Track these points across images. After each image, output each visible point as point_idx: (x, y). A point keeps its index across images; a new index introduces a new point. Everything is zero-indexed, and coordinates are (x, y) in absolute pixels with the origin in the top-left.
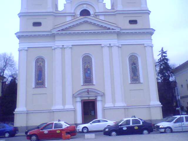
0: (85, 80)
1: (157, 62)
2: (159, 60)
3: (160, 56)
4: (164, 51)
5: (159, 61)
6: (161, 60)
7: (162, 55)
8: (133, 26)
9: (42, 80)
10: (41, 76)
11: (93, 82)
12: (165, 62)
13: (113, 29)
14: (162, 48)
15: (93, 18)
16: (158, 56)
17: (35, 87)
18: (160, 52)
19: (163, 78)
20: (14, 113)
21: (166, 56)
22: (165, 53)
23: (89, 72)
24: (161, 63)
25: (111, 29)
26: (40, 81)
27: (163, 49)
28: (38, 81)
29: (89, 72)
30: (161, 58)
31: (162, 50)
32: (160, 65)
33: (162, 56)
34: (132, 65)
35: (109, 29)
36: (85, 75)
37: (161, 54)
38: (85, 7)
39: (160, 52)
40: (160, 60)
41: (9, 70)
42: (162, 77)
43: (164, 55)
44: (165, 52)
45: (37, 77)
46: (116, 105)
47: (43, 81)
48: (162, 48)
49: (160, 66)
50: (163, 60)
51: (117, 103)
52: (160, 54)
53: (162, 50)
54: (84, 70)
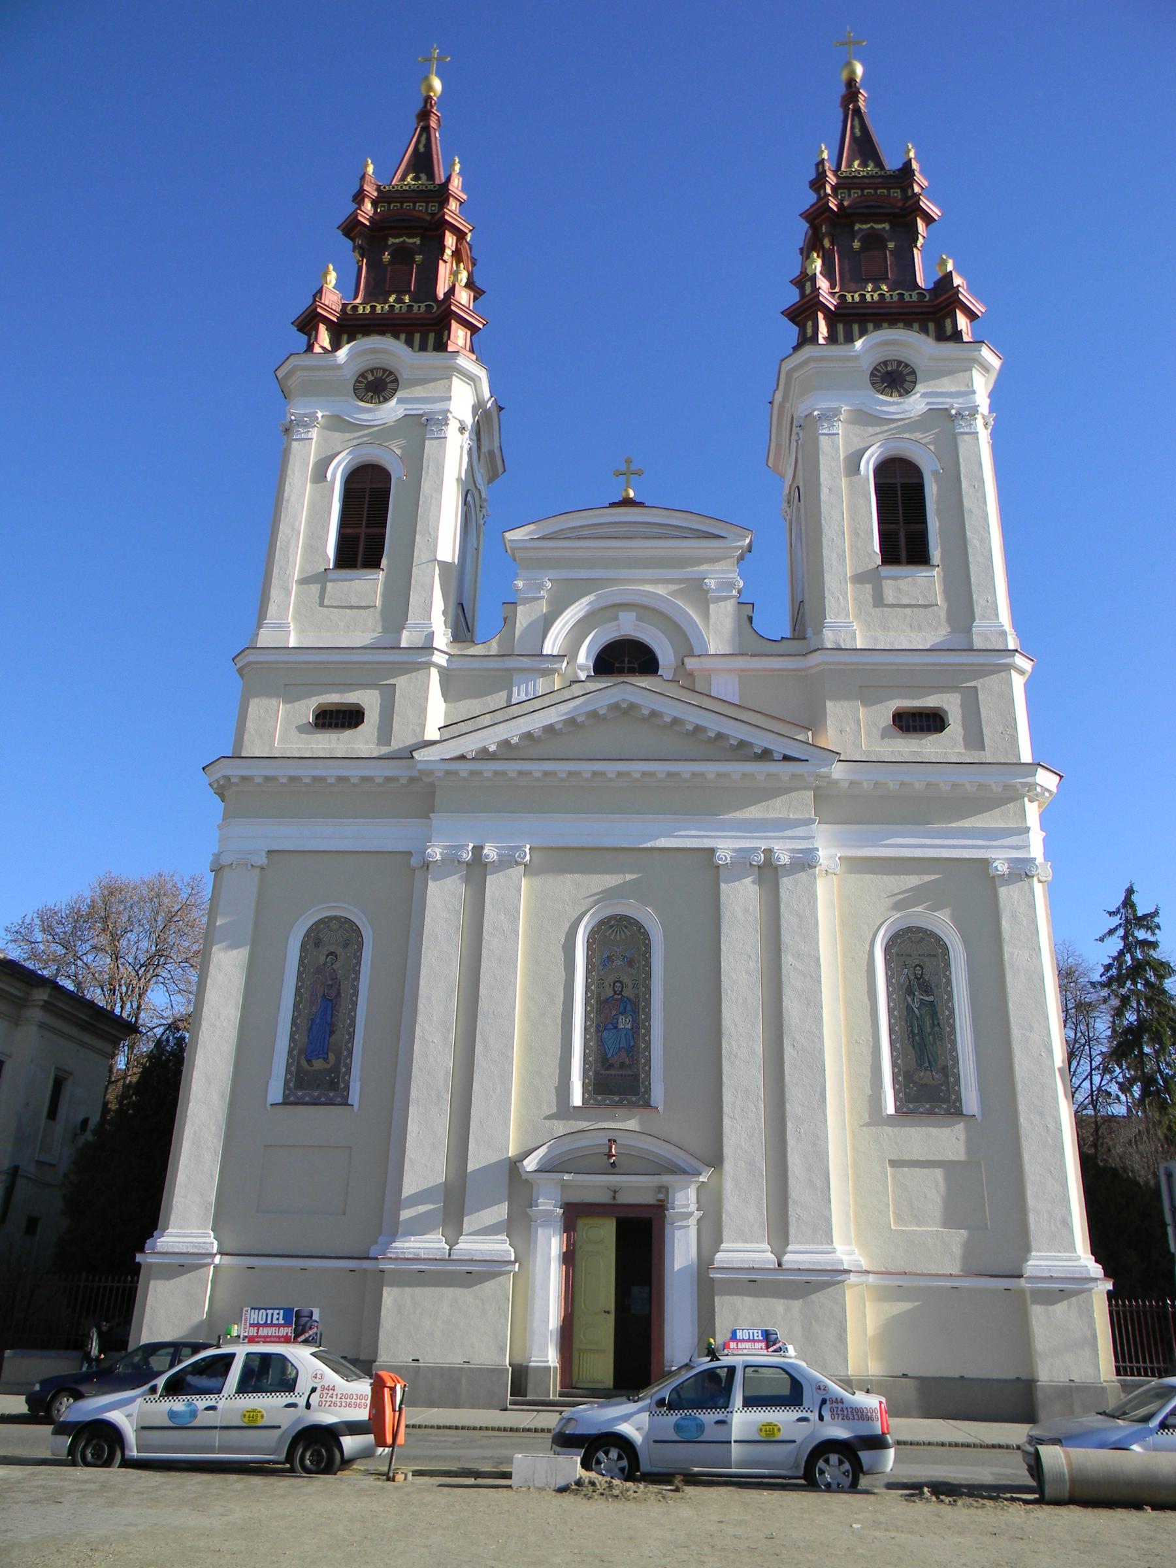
0: (597, 1074)
1: (1093, 984)
2: (1108, 967)
3: (1115, 944)
4: (1139, 914)
5: (1111, 979)
6: (1120, 968)
7: (1124, 938)
8: (929, 746)
9: (331, 1056)
10: (332, 1033)
11: (648, 1090)
12: (1148, 984)
13: (786, 758)
14: (1130, 891)
15: (672, 690)
16: (1101, 940)
17: (285, 1096)
18: (1111, 914)
19: (1136, 1091)
20: (139, 1258)
21: (1154, 945)
22: (1147, 921)
23: (625, 1023)
24: (1123, 991)
25: (284, 780)
26: (318, 1064)
27: (1134, 898)
28: (309, 1062)
29: (625, 1023)
30: (1121, 953)
31: (1128, 903)
32: (1115, 1002)
33: (1129, 946)
34: (910, 992)
35: (765, 755)
36: (601, 1042)
37: (1121, 932)
38: (628, 627)
39: (1111, 914)
40: (1114, 972)
41: (172, 987)
42: (1132, 1081)
43: (1141, 934)
44: (1145, 917)
45: (302, 1038)
46: (789, 1259)
47: (336, 1068)
48: (1130, 891)
49: (1119, 1013)
50: (1138, 969)
51: (1038, 1254)
52: (1111, 932)
53: (1128, 903)
54: (599, 1011)
